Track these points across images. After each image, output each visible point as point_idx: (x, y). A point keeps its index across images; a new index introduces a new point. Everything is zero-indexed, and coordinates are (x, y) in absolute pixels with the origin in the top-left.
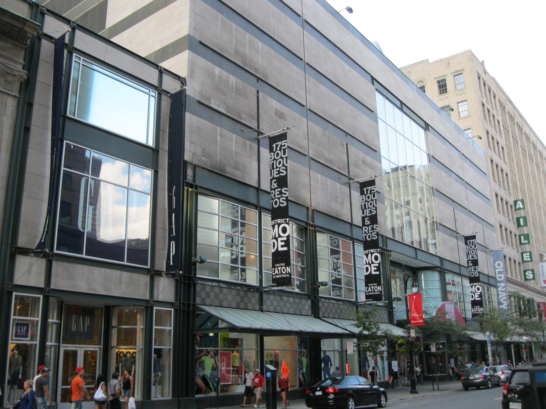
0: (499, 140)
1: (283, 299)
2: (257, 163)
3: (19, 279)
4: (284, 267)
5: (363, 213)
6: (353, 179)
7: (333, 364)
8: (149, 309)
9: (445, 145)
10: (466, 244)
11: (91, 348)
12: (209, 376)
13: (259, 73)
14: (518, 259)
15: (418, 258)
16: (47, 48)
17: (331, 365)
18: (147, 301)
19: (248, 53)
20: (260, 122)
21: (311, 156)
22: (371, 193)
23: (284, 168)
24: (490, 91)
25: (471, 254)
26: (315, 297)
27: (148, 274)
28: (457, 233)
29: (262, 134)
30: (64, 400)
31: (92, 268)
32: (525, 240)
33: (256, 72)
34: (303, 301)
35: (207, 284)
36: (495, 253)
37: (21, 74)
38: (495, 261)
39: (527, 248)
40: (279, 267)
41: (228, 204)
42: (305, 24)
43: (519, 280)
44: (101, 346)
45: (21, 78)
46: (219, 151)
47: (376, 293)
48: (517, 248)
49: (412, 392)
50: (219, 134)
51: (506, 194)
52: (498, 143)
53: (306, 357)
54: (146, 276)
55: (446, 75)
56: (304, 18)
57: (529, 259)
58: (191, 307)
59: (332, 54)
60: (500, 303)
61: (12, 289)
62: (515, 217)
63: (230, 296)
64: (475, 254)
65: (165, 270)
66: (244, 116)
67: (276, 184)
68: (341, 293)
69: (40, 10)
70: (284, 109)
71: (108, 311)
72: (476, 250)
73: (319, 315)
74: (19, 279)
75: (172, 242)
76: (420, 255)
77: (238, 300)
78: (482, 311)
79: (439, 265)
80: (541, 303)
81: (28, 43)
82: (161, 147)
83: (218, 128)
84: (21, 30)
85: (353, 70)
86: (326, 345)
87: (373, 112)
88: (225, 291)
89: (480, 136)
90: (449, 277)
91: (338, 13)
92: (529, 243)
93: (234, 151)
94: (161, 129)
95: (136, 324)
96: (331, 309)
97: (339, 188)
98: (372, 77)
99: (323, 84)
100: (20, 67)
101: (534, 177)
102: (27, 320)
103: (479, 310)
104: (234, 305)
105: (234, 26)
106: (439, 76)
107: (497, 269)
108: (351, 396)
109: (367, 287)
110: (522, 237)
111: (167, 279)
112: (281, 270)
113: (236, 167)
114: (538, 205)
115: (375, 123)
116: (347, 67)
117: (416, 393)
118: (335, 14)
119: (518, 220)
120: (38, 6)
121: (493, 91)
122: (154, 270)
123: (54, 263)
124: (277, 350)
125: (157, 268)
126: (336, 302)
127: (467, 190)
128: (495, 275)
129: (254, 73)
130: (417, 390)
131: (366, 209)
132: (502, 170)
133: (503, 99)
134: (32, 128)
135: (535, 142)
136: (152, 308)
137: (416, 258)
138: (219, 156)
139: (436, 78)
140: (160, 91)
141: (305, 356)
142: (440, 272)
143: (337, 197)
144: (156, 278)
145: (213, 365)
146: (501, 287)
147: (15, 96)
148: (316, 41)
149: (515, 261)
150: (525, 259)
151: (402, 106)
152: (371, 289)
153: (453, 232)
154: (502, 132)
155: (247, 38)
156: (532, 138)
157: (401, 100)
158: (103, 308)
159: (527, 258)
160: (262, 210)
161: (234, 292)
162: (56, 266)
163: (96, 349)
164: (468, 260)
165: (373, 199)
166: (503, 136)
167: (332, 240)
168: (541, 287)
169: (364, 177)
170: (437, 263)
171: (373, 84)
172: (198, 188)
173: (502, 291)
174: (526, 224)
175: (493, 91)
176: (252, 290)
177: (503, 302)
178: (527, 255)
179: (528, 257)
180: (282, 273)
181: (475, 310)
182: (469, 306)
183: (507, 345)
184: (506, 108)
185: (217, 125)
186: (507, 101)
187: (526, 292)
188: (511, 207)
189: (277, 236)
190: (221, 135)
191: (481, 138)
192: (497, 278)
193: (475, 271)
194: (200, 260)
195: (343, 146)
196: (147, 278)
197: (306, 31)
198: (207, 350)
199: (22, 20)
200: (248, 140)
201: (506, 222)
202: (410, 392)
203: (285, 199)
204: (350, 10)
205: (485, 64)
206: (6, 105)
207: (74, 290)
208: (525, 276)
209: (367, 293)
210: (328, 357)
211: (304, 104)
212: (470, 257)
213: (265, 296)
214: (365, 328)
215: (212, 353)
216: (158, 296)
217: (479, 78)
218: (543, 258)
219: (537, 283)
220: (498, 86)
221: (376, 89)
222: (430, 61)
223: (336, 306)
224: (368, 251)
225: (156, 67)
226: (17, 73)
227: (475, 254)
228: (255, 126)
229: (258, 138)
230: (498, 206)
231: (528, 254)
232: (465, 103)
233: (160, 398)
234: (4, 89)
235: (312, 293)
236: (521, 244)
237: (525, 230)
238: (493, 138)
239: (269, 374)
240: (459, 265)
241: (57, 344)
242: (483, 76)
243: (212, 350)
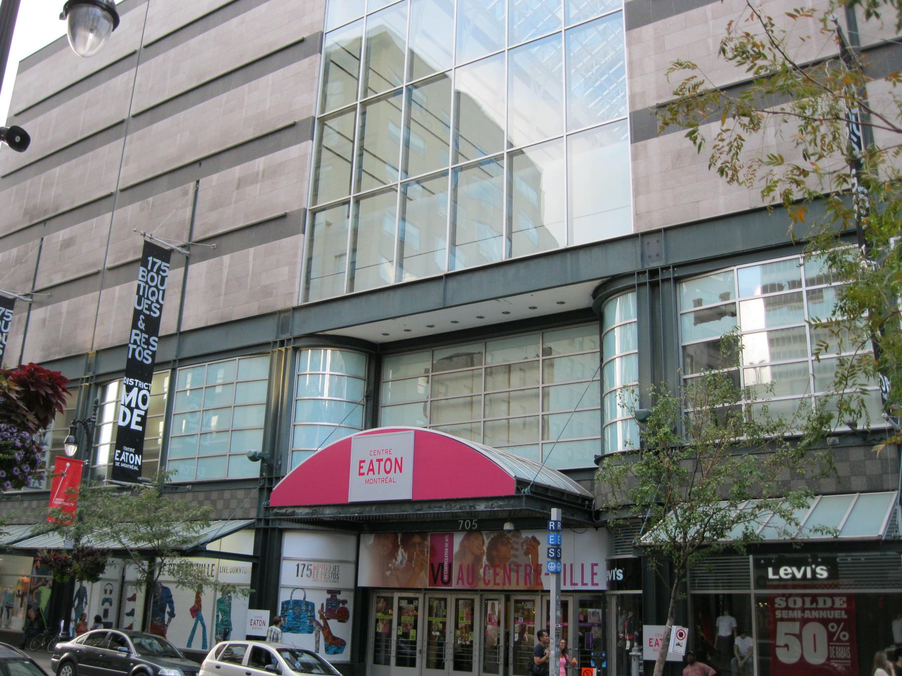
4: (132, 455)
5: (139, 304)
17: (86, 603)
22: (158, 273)
25: (148, 299)
47: (131, 467)
72: (161, 292)
78: (138, 465)
109: (119, 451)
141: (48, 586)
164: (139, 308)
165: (160, 287)
180: (128, 463)
189: (133, 405)
193: (146, 347)
198: (45, 578)
203: (150, 353)
209: (118, 461)
212: (144, 306)
224: (135, 382)
227: (157, 301)
241: (540, 593)
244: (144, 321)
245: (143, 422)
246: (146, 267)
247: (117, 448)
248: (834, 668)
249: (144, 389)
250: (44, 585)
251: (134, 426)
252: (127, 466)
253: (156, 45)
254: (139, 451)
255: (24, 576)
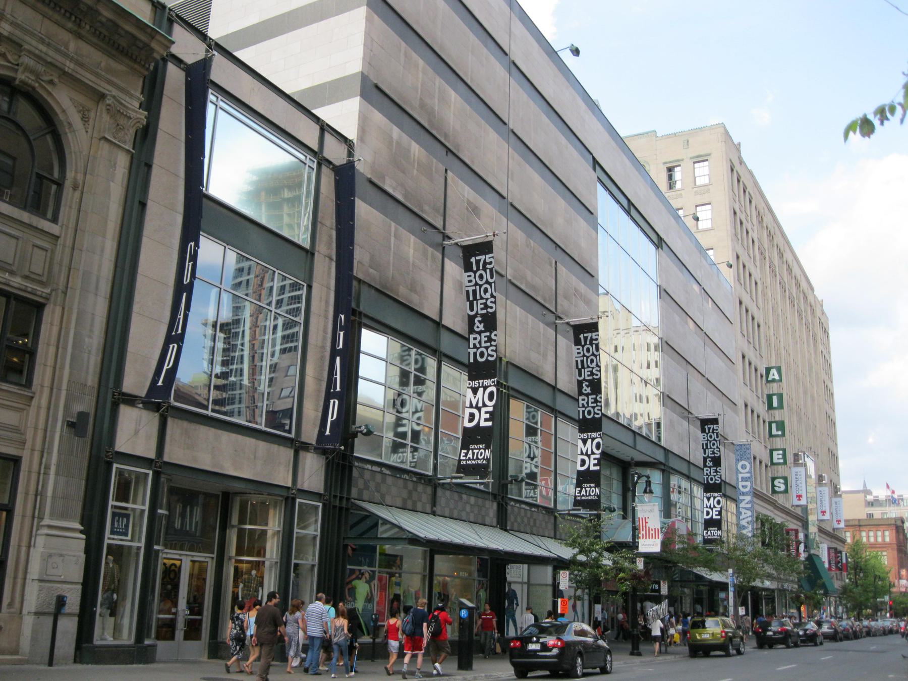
0: (753, 271)
1: (461, 498)
2: (440, 283)
3: (122, 444)
4: (482, 451)
6: (561, 318)
7: (520, 603)
8: (290, 501)
9: (682, 272)
10: (703, 431)
11: (200, 556)
12: (360, 611)
13: (449, 142)
14: (766, 459)
15: (638, 447)
16: (175, 77)
17: (517, 605)
18: (288, 488)
19: (436, 108)
20: (447, 219)
21: (509, 277)
23: (493, 300)
24: (745, 191)
26: (503, 498)
27: (291, 447)
28: (690, 413)
29: (450, 238)
30: (187, 637)
31: (220, 432)
32: (777, 430)
33: (445, 139)
34: (488, 504)
35: (366, 467)
36: (738, 448)
37: (139, 116)
38: (737, 461)
39: (778, 443)
40: (476, 449)
41: (397, 346)
42: (512, 66)
43: (765, 492)
44: (215, 556)
45: (139, 122)
46: (391, 261)
48: (765, 441)
49: (632, 654)
50: (393, 234)
51: (756, 357)
52: (750, 275)
53: (486, 591)
54: (288, 449)
55: (682, 160)
56: (512, 58)
57: (781, 461)
58: (344, 502)
59: (545, 120)
60: (740, 527)
61: (112, 458)
62: (766, 392)
63: (395, 488)
64: (717, 447)
65: (314, 443)
66: (426, 208)
67: (482, 324)
68: (535, 494)
69: (167, 14)
70: (480, 201)
71: (227, 498)
73: (506, 527)
74: (122, 444)
75: (332, 401)
76: (641, 445)
77: (405, 495)
79: (663, 460)
80: (792, 530)
81: (152, 68)
82: (317, 248)
83: (393, 224)
84: (147, 46)
85: (570, 146)
86: (515, 574)
87: (592, 213)
88: (390, 480)
89: (731, 262)
90: (675, 480)
91: (556, 53)
92: (783, 435)
93: (411, 262)
94: (319, 220)
95: (266, 524)
96: (529, 519)
97: (542, 330)
98: (594, 159)
99: (530, 165)
100: (137, 104)
101: (794, 332)
102: (126, 509)
103: (714, 533)
104: (399, 502)
105: (421, 63)
106: (671, 159)
107: (741, 473)
108: (580, 654)
110: (774, 426)
111: (315, 456)
112: (478, 453)
113: (413, 288)
114: (796, 376)
115: (594, 232)
116: (563, 140)
117: (639, 654)
118: (552, 53)
119: (770, 397)
120: (163, 7)
121: (749, 193)
122: (299, 441)
123: (170, 421)
124: (448, 577)
125: (304, 439)
126: (528, 508)
127: (706, 347)
128: (738, 483)
129: (442, 140)
130: (640, 650)
131: (584, 368)
132: (753, 319)
133: (761, 206)
134: (150, 203)
135: (799, 278)
136: (294, 499)
137: (634, 448)
138: (391, 268)
139: (665, 163)
140: (322, 161)
142: (663, 471)
143: (539, 344)
144: (302, 454)
145: (368, 594)
146: (746, 501)
147: (128, 151)
148: (525, 96)
149: (761, 462)
150: (775, 461)
151: (630, 208)
152: (586, 491)
153: (684, 411)
154: (758, 258)
155: (437, 84)
156: (796, 270)
157: (629, 197)
158: (219, 495)
159: (778, 459)
160: (443, 358)
161: (401, 482)
162: (174, 427)
163: (207, 560)
164: (706, 456)
165: (491, 280)
166: (758, 264)
167: (529, 413)
168: (793, 506)
169: (578, 317)
170: (660, 457)
171: (595, 170)
172: (363, 318)
173: (745, 508)
174: (781, 406)
175: (749, 193)
176: (423, 482)
177: (746, 525)
178: (778, 454)
179: (781, 456)
180: (477, 459)
181: (709, 533)
182: (700, 528)
183: (755, 591)
184: (765, 219)
185: (391, 220)
186: (766, 210)
187: (772, 511)
188: (762, 376)
190: (395, 236)
191: (731, 266)
192: (740, 487)
194: (365, 431)
195: (551, 265)
196: (290, 453)
197: (514, 79)
198: (360, 570)
199: (149, 31)
200: (430, 246)
201: (754, 402)
202: (628, 653)
204: (576, 52)
205: (742, 149)
206: (115, 164)
207: (193, 466)
208: (773, 486)
210: (514, 592)
211: (505, 194)
212: (709, 452)
213: (440, 492)
214: (582, 552)
215: (367, 575)
216: (302, 484)
217: (732, 170)
218: (798, 460)
219: (787, 499)
220: (756, 184)
221: (598, 178)
222: (659, 134)
223: (529, 513)
224: (479, 383)
225: (315, 120)
226: (133, 115)
228: (439, 224)
229: (442, 244)
230: (744, 374)
231: (781, 452)
232: (709, 207)
233: (110, 640)
234: (115, 138)
235: (499, 491)
236: (771, 435)
237: (777, 415)
238: (744, 266)
239: (464, 613)
240: (689, 462)
242: (737, 167)
243: (367, 571)
244: (587, 386)
245: (720, 513)
246: (471, 270)
247: (705, 529)
248: (174, 522)
249: (491, 386)
250: (359, 578)
251: (715, 517)
252: (474, 462)
253: (424, 46)
254: (720, 528)
255: (445, 576)
